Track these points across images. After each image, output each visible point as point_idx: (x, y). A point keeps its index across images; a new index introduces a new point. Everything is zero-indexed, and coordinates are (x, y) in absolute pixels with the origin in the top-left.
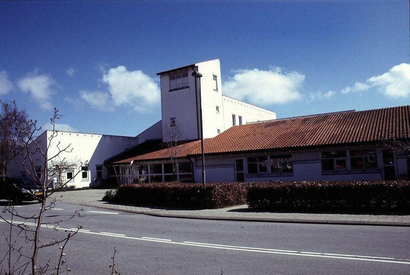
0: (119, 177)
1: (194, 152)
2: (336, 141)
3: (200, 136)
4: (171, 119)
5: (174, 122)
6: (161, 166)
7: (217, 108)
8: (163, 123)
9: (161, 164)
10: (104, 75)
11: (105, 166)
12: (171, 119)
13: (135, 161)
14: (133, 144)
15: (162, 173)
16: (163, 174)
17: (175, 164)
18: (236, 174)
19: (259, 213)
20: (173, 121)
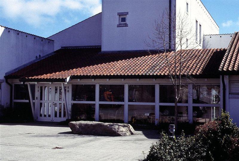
0: (34, 103)
1: (228, 82)
2: (197, 72)
3: (171, 48)
4: (120, 14)
5: (124, 20)
6: (94, 92)
7: (187, 4)
8: (105, 20)
9: (94, 86)
10: (5, 107)
11: (7, 82)
12: (120, 14)
13: (73, 78)
14: (48, 50)
15: (94, 100)
16: (97, 102)
17: (227, 117)
18: (92, 82)
19: (92, 102)
20: (123, 18)
